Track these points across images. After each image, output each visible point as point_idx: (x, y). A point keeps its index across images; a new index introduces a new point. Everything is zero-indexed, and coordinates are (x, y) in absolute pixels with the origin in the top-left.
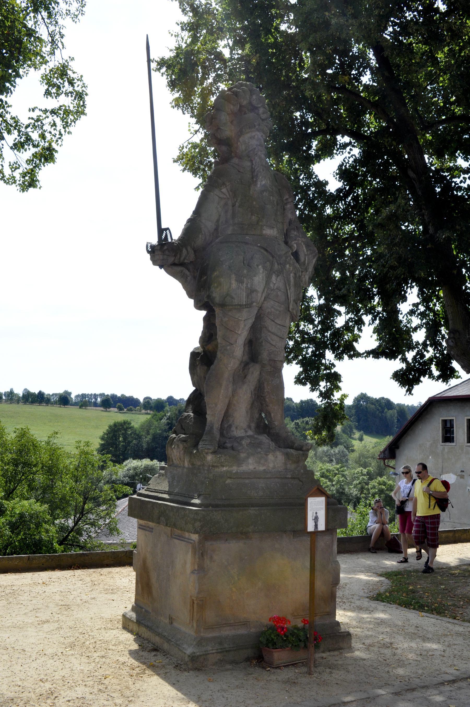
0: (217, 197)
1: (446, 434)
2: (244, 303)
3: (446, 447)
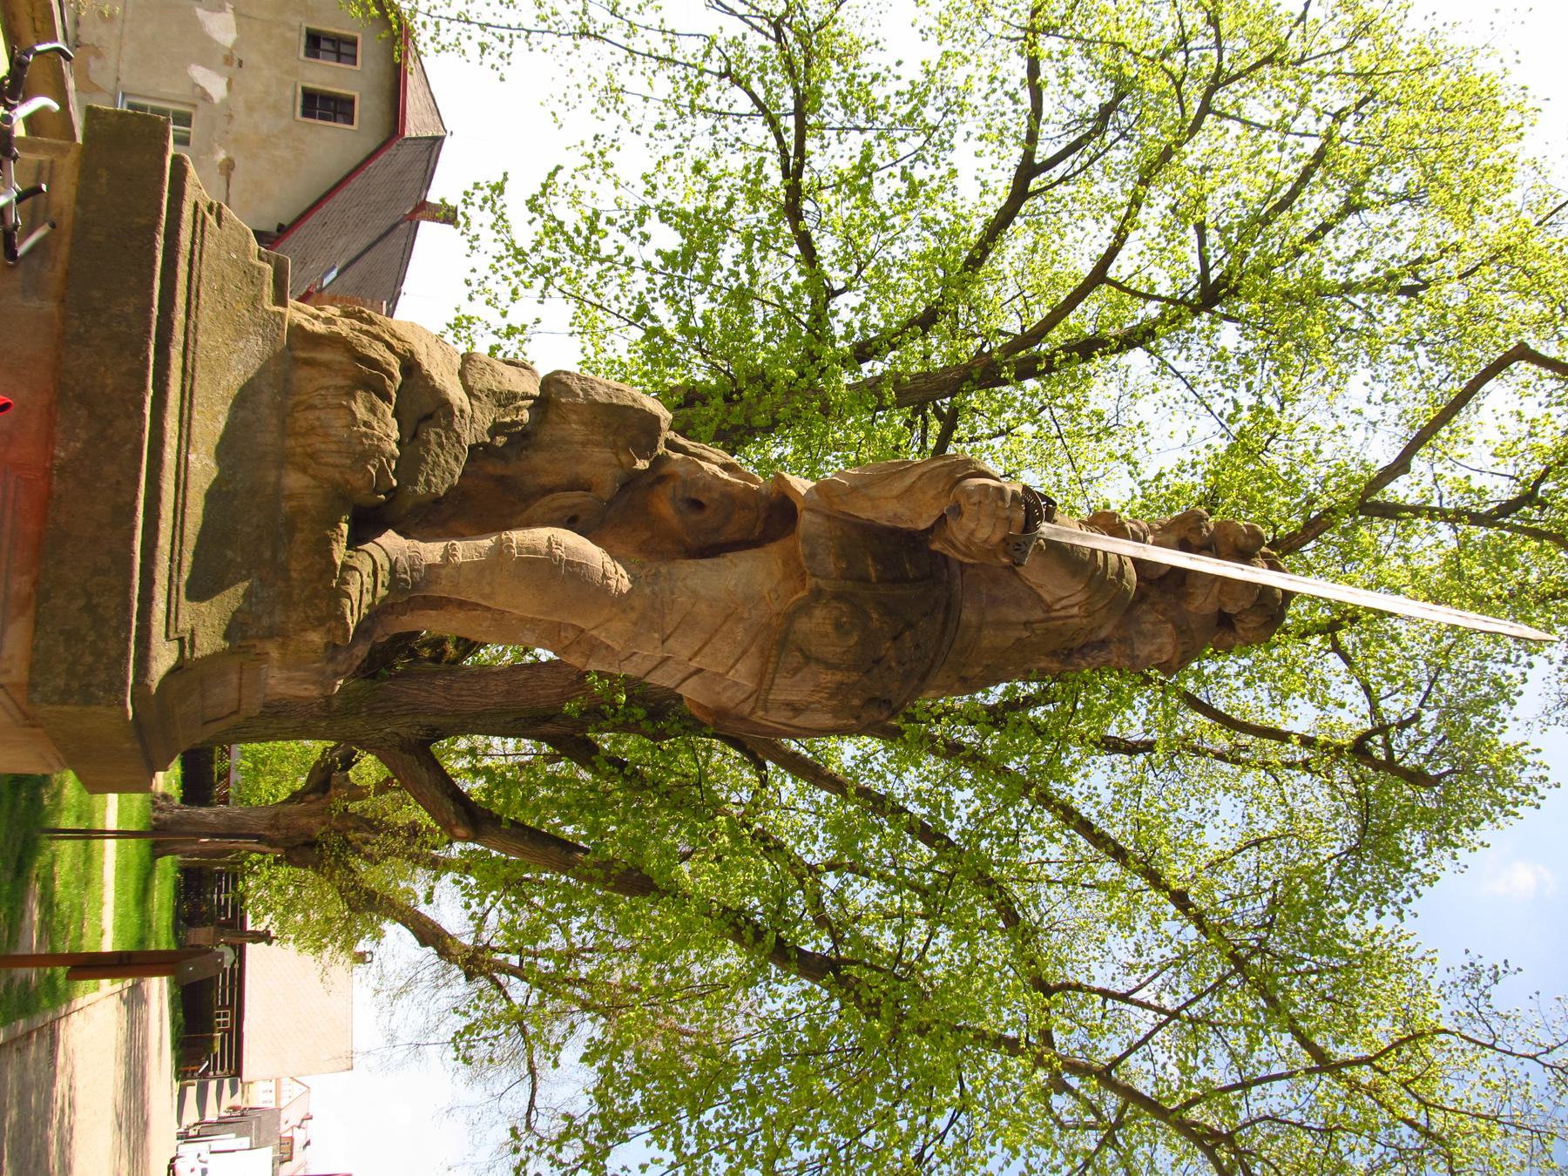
3: (296, 35)
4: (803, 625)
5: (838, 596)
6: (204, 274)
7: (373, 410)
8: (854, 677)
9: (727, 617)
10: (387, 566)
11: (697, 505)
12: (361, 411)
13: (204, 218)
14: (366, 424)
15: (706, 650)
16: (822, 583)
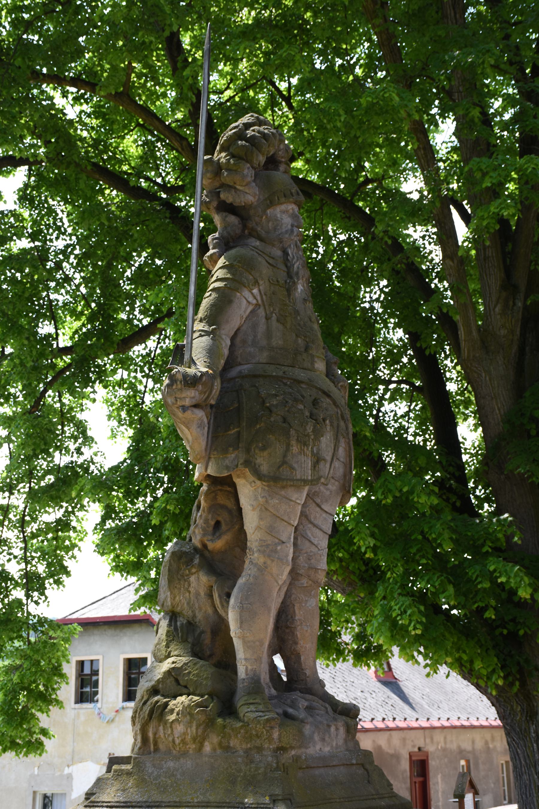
0: (245, 301)
1: (82, 688)
2: (310, 478)
3: (82, 711)
4: (264, 468)
5: (248, 450)
6: (116, 800)
7: (172, 711)
8: (292, 432)
9: (266, 509)
10: (245, 698)
11: (218, 524)
12: (173, 717)
13: (91, 802)
14: (178, 714)
15: (286, 518)
16: (241, 461)
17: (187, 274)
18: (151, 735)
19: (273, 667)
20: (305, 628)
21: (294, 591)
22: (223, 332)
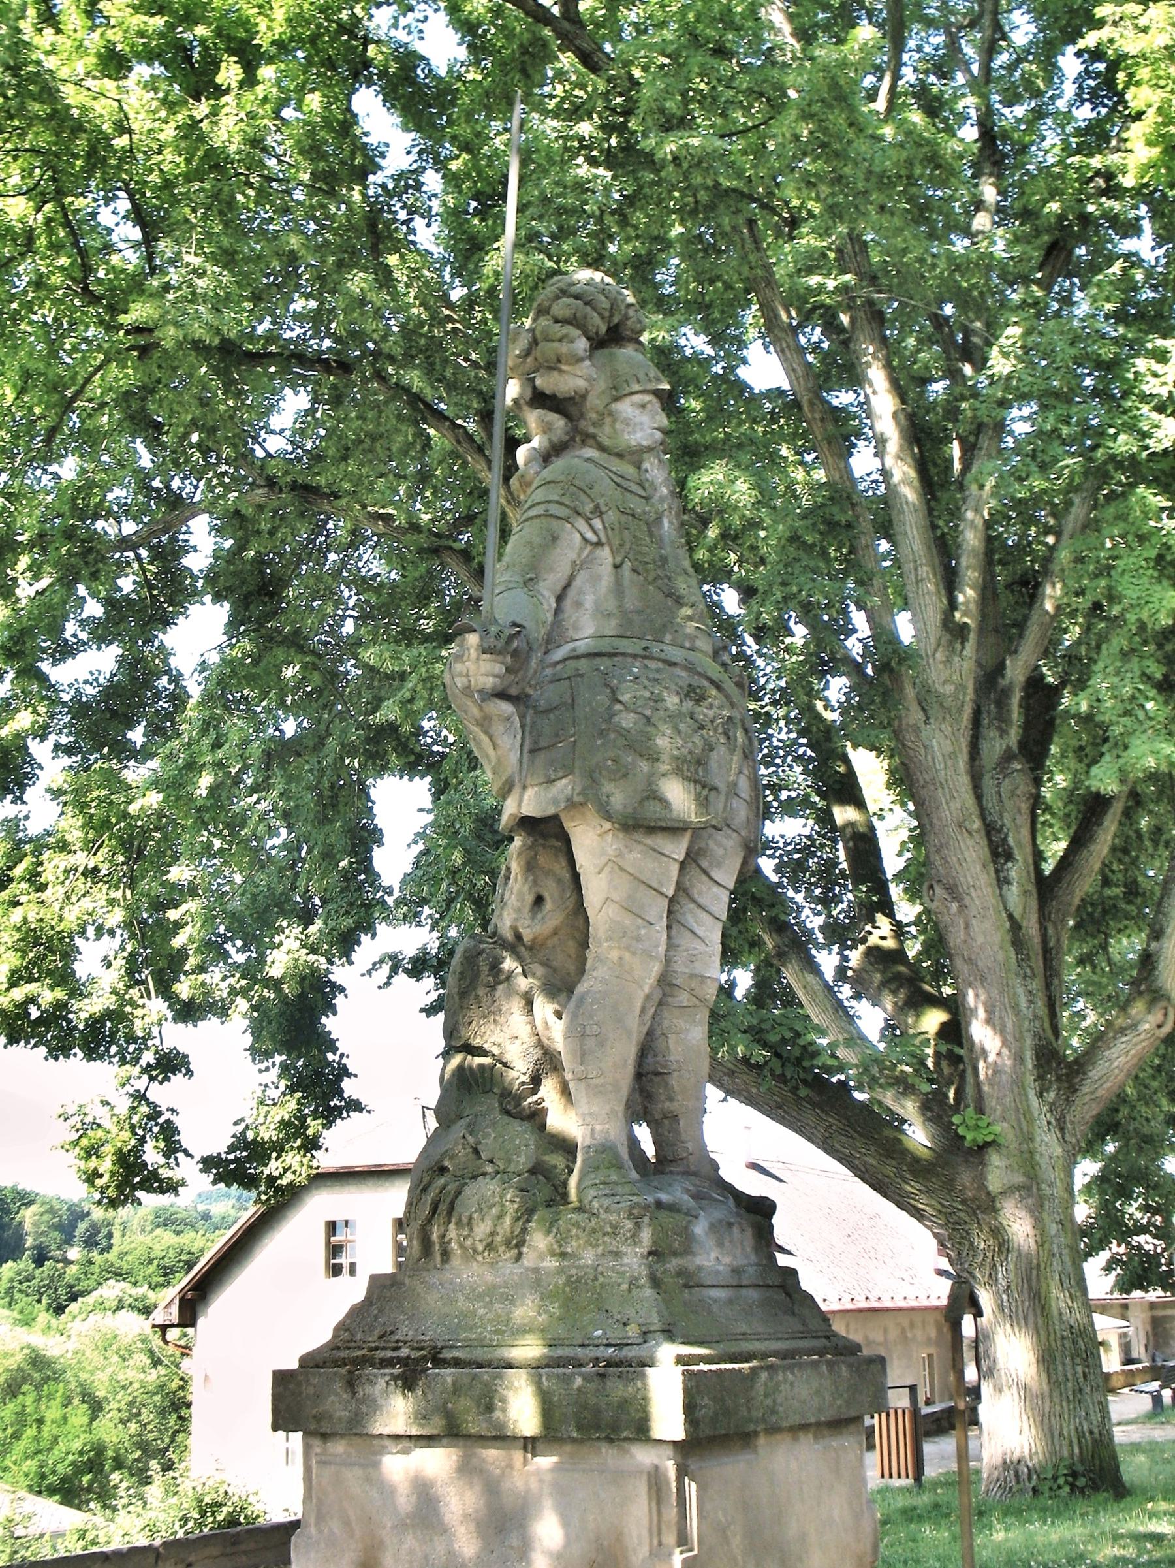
11: (539, 900)
17: (575, 1162)
18: (435, 1237)
19: (634, 1143)
20: (687, 1075)
21: (666, 1014)
22: (542, 584)
